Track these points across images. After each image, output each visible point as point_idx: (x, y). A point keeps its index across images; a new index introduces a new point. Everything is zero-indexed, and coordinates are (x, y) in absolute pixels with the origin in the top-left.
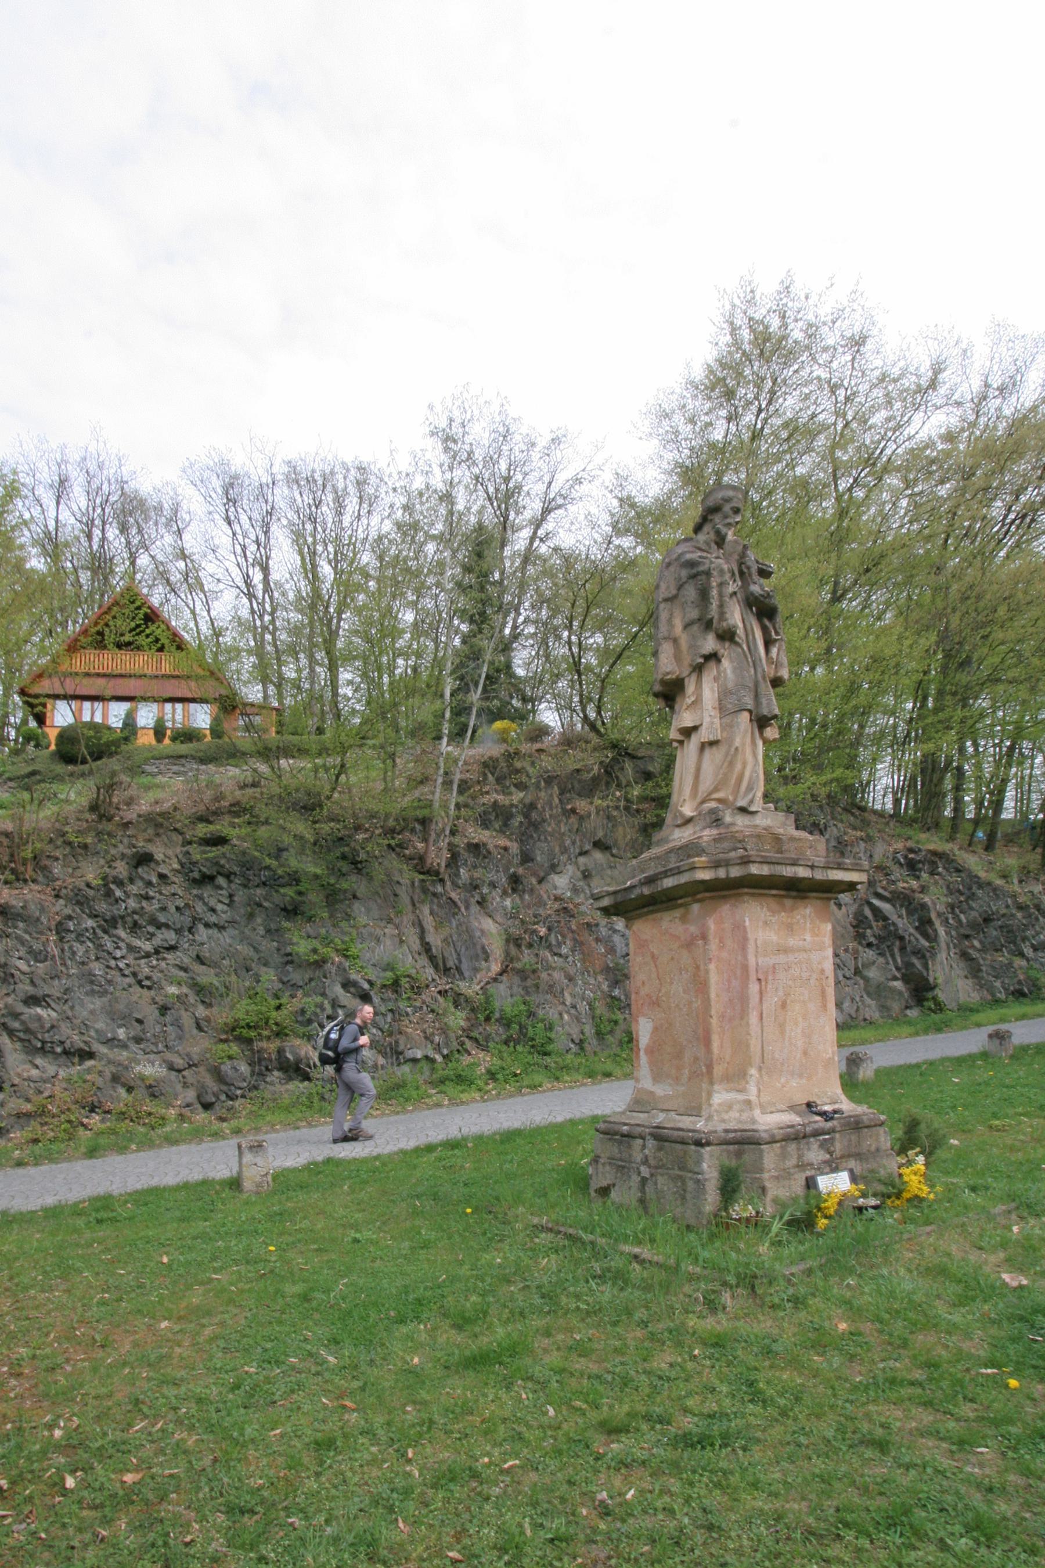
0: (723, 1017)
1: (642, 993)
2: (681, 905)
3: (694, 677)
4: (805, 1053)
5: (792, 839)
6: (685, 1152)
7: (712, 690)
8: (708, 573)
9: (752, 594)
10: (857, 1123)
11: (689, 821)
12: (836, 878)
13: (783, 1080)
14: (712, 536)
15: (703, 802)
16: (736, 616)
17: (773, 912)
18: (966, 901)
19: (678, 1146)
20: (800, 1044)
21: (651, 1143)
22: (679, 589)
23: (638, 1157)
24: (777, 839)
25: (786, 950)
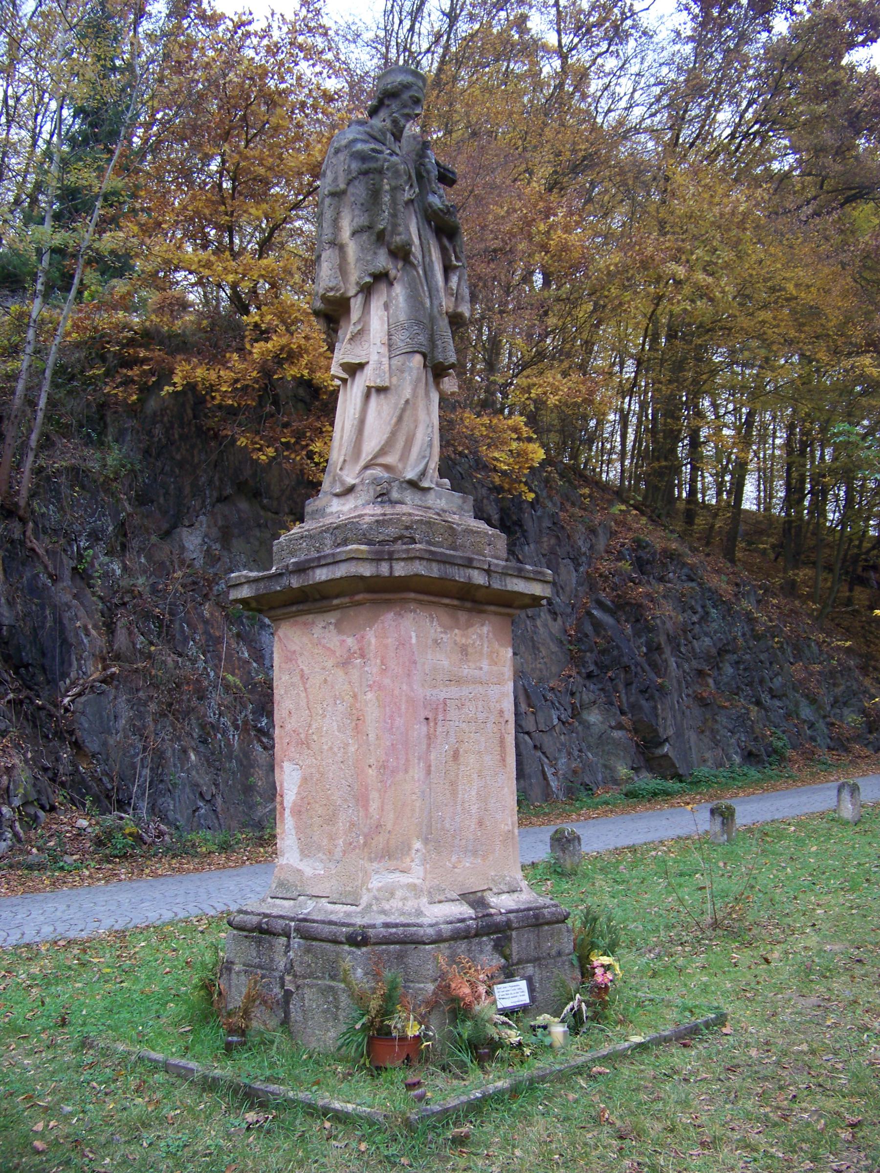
0: (384, 767)
1: (288, 727)
2: (337, 607)
3: (360, 298)
4: (480, 823)
5: (469, 531)
6: (338, 954)
7: (381, 318)
8: (380, 172)
9: (430, 205)
10: (536, 917)
11: (350, 490)
12: (516, 589)
13: (454, 859)
14: (388, 124)
15: (366, 467)
16: (413, 229)
17: (446, 629)
18: (699, 623)
19: (328, 946)
20: (474, 809)
21: (296, 942)
22: (348, 184)
23: (281, 963)
24: (451, 529)
25: (457, 680)
